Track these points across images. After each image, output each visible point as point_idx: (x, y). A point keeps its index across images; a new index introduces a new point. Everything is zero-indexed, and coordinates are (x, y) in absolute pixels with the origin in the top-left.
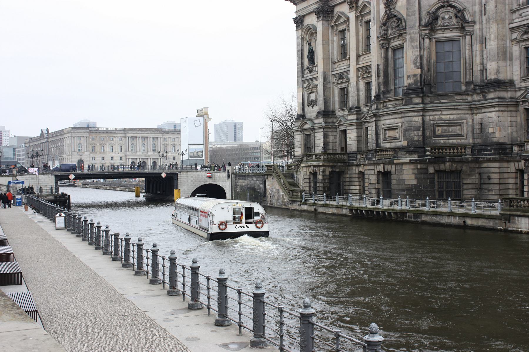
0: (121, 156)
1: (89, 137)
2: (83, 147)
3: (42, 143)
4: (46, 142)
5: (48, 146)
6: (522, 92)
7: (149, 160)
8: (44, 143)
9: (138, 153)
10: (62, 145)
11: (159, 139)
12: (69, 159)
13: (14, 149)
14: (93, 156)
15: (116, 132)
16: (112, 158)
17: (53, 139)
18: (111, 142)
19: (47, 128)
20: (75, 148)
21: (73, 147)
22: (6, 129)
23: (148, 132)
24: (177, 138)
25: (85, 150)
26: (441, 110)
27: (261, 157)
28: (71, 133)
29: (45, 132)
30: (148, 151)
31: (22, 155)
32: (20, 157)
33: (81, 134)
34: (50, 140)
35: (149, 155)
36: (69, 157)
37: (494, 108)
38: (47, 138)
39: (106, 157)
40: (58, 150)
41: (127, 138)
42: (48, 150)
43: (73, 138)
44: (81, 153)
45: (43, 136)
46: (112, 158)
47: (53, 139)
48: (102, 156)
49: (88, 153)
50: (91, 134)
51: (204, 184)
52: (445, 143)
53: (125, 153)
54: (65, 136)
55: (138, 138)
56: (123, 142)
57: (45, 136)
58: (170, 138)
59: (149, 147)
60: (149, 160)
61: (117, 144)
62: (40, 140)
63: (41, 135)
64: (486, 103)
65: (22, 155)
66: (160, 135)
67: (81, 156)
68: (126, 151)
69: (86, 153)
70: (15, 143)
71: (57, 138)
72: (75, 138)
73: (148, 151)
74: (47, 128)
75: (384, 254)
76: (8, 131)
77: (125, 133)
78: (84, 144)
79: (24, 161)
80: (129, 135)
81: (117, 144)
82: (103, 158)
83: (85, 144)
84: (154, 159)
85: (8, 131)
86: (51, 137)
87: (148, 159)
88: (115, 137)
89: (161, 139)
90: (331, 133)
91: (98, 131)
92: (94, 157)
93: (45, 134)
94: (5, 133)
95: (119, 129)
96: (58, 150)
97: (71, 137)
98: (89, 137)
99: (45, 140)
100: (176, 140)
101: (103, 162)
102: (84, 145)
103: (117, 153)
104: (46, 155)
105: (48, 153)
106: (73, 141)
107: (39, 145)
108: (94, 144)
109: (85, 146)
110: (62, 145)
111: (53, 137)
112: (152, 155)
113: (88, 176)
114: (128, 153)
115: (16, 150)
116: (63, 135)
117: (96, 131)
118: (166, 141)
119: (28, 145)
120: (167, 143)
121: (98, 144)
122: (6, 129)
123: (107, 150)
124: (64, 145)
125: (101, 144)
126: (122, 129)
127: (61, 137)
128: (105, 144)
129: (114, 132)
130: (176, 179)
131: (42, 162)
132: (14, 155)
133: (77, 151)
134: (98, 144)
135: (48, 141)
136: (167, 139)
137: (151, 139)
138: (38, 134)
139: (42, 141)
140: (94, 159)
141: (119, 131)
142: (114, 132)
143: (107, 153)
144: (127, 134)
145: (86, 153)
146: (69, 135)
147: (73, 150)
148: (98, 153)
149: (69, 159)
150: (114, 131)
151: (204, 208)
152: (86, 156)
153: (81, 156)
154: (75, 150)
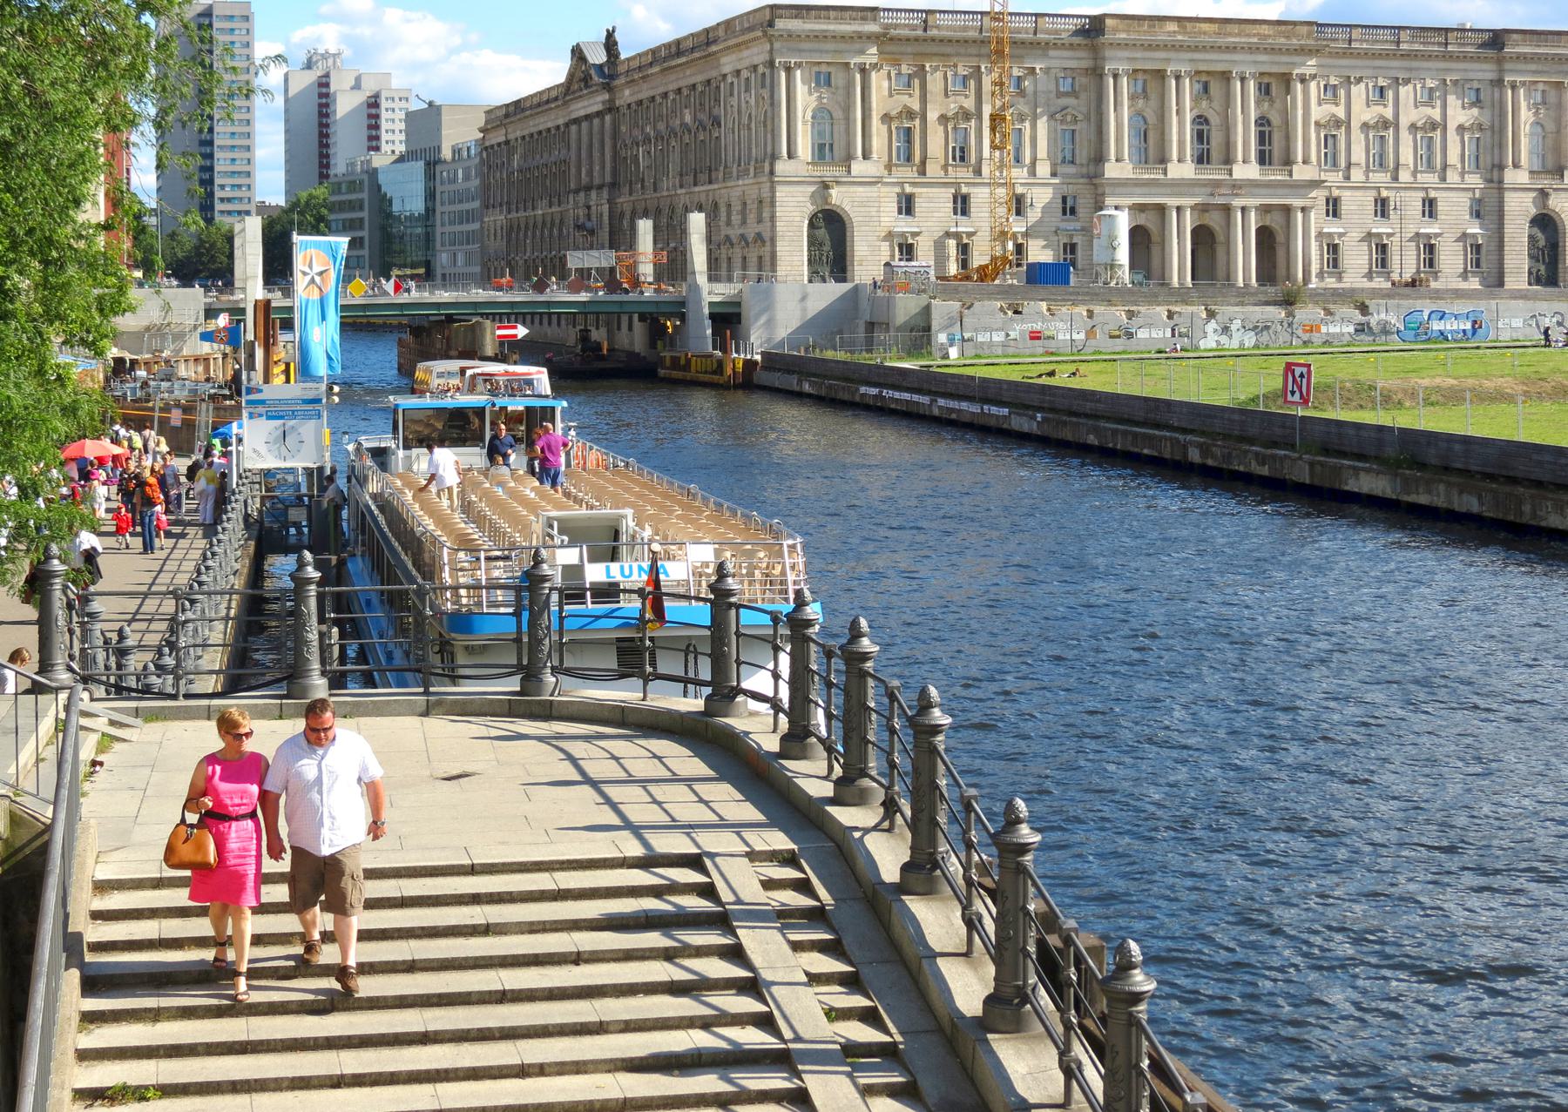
3: (577, 121)
4: (599, 114)
6: (976, 938)
8: (588, 117)
10: (703, 117)
12: (752, 206)
19: (610, 35)
29: (598, 57)
31: (590, 173)
34: (626, 96)
37: (1080, 1065)
38: (608, 87)
39: (980, 196)
40: (675, 158)
63: (571, 76)
64: (579, 140)
65: (590, 173)
74: (610, 35)
79: (476, 226)
96: (675, 158)
104: (600, 187)
112: (1252, 185)
124: (716, 122)
132: (430, 195)
135: (611, 108)
137: (1252, 85)
140: (907, 206)
149: (752, 206)
151: (327, 821)
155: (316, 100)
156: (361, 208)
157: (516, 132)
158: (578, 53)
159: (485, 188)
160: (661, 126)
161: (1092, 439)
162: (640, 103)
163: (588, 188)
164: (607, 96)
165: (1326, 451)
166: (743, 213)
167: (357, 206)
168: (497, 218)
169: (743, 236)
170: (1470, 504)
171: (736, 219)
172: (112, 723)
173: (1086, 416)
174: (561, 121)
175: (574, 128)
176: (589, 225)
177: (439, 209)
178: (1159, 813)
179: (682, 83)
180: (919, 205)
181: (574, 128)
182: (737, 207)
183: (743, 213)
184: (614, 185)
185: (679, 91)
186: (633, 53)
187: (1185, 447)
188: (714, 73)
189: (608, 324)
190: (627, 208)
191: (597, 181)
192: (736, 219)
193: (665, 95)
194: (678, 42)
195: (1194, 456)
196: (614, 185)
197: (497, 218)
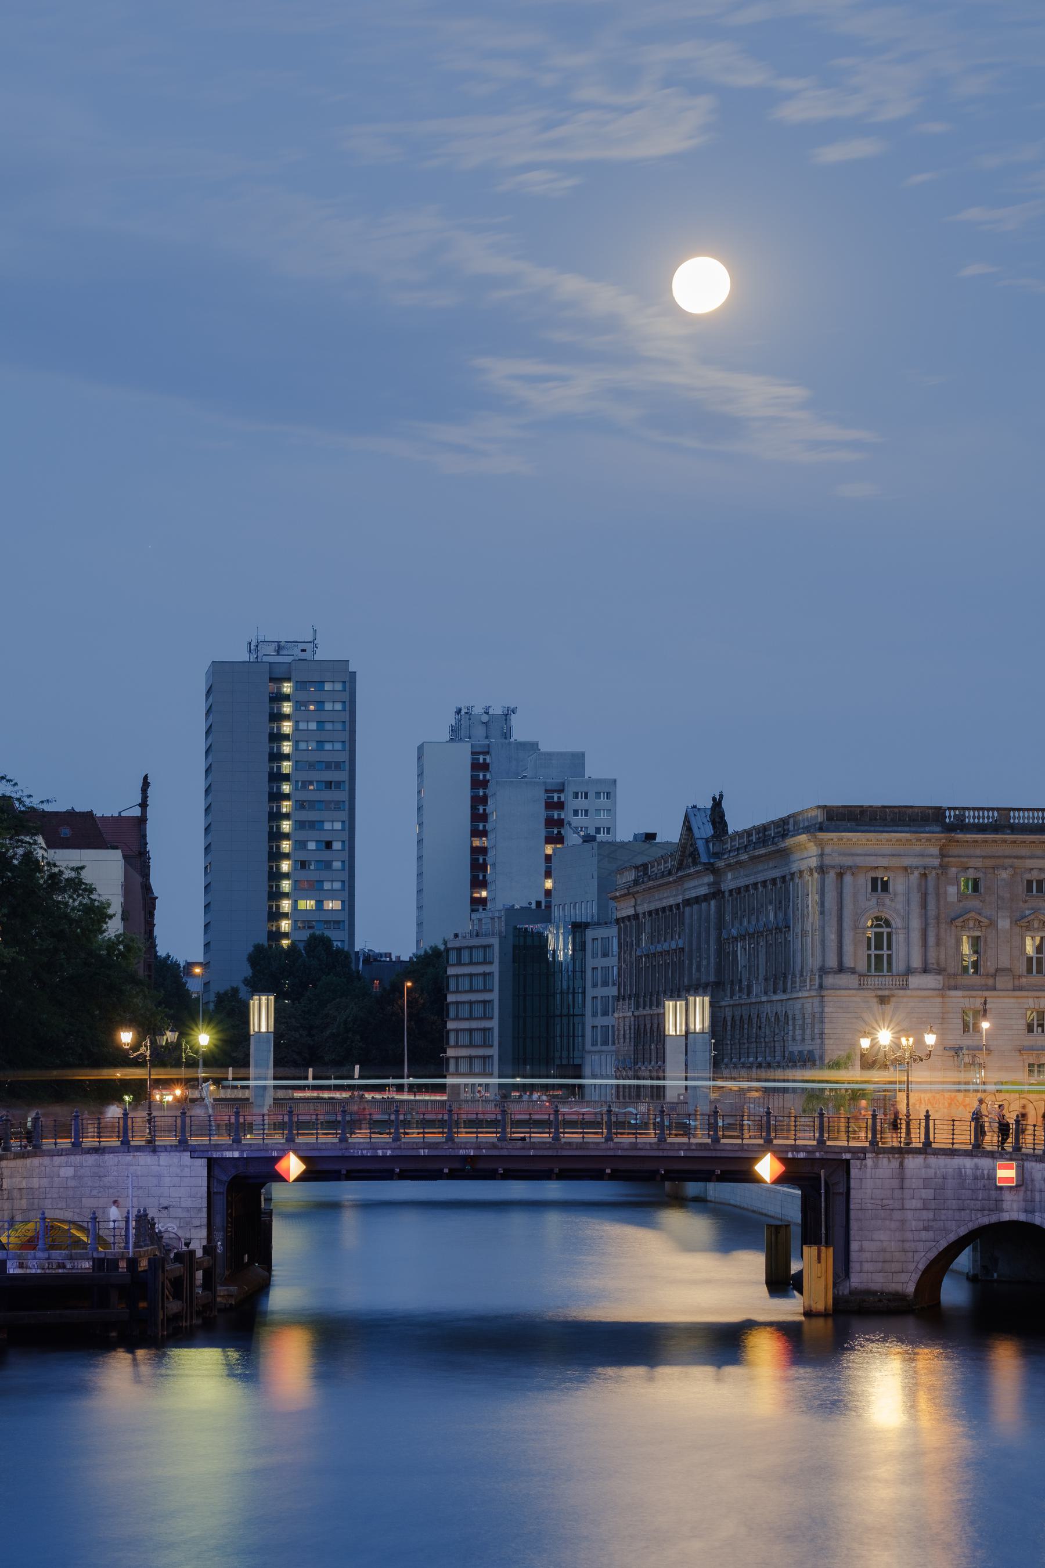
2: (899, 939)
4: (706, 898)
5: (721, 925)
19: (717, 803)
20: (848, 948)
22: (593, 770)
25: (916, 962)
26: (574, 1036)
29: (704, 830)
38: (711, 868)
45: (694, 855)
51: (986, 1221)
52: (634, 1146)
76: (608, 789)
78: (907, 918)
83: (916, 924)
85: (608, 789)
90: (145, 1114)
93: (700, 844)
94: (581, 803)
99: (699, 886)
102: (907, 928)
109: (916, 936)
113: (411, 1166)
121: (1004, 924)
122: (593, 770)
130: (842, 1189)
133: (862, 966)
135: (717, 894)
147: (832, 962)
154: (848, 962)
164: (710, 878)
179: (760, 878)
194: (764, 828)
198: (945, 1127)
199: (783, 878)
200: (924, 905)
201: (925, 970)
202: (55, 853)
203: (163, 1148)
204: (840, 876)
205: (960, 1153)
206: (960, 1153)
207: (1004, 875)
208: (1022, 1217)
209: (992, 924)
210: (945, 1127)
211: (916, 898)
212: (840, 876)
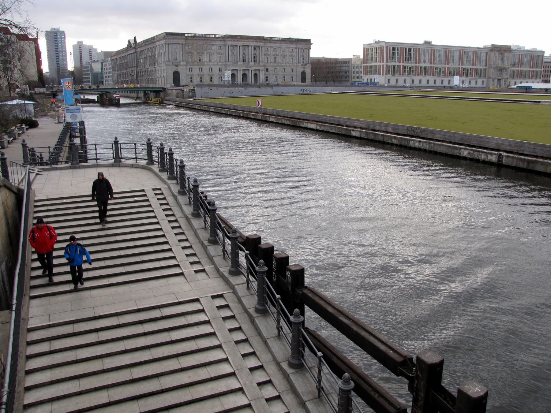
0: (220, 67)
1: (185, 44)
3: (129, 54)
4: (133, 53)
7: (250, 71)
8: (131, 54)
9: (239, 63)
10: (153, 54)
11: (261, 48)
12: (162, 70)
13: (102, 63)
14: (190, 67)
15: (215, 39)
16: (211, 69)
17: (142, 49)
18: (209, 50)
19: (135, 38)
21: (167, 56)
23: (249, 40)
24: (279, 47)
25: (182, 60)
27: (350, 72)
28: (165, 39)
30: (249, 62)
31: (132, 64)
32: (108, 75)
33: (176, 40)
34: (139, 50)
35: (250, 67)
36: (162, 68)
40: (148, 61)
41: (227, 47)
42: (137, 61)
43: (167, 45)
44: (177, 64)
46: (211, 69)
47: (142, 49)
48: (200, 67)
49: (184, 63)
50: (187, 41)
53: (224, 63)
54: (157, 44)
55: (238, 47)
56: (223, 51)
57: (133, 46)
58: (272, 47)
59: (250, 57)
60: (250, 71)
61: (215, 54)
62: (127, 51)
63: (128, 46)
65: (132, 64)
66: (262, 44)
67: (177, 66)
68: (226, 61)
69: (182, 63)
70: (102, 58)
71: (147, 47)
72: (170, 45)
73: (249, 62)
74: (135, 38)
75: (393, 155)
77: (224, 41)
78: (180, 52)
79: (111, 74)
80: (229, 43)
81: (215, 54)
82: (201, 69)
83: (181, 53)
84: (255, 70)
86: (139, 47)
87: (248, 70)
88: (213, 45)
89: (263, 48)
91: (195, 38)
92: (191, 68)
95: (218, 36)
96: (148, 61)
97: (165, 44)
98: (185, 44)
99: (133, 51)
100: (278, 49)
101: (201, 73)
102: (180, 54)
103: (216, 63)
104: (134, 67)
105: (137, 64)
106: (167, 49)
107: (126, 56)
108: (191, 53)
110: (153, 54)
111: (142, 46)
112: (253, 66)
114: (228, 63)
115: (103, 64)
116: (154, 42)
117: (193, 38)
118: (268, 51)
119: (114, 58)
120: (269, 53)
121: (195, 53)
123: (205, 60)
124: (155, 55)
125: (198, 53)
126: (220, 36)
127: (151, 46)
128: (204, 53)
129: (213, 39)
131: (130, 75)
132: (102, 68)
134: (195, 53)
135: (136, 52)
136: (269, 49)
137: (252, 48)
138: (125, 45)
139: (130, 52)
141: (218, 38)
142: (213, 39)
143: (206, 63)
144: (227, 42)
145: (182, 63)
146: (163, 42)
148: (196, 63)
149: (162, 70)
150: (212, 38)
152: (182, 67)
153: (177, 66)
154: (170, 60)
155: (79, 50)
156: (89, 68)
157: (118, 57)
158: (129, 41)
159: (113, 67)
160: (145, 56)
161: (224, 112)
162: (141, 51)
163: (132, 67)
165: (264, 114)
166: (161, 71)
167: (88, 74)
168: (115, 73)
169: (161, 76)
170: (288, 122)
171: (160, 73)
172: (38, 171)
173: (223, 108)
174: (126, 55)
175: (129, 56)
176: (132, 74)
177: (104, 71)
178: (476, 234)
179: (149, 47)
180: (193, 70)
181: (129, 56)
182: (160, 70)
183: (161, 71)
184: (137, 67)
185: (148, 49)
186: (141, 41)
187: (240, 113)
188: (155, 46)
189: (137, 93)
190: (139, 71)
191: (134, 66)
192: (160, 73)
193: (146, 50)
195: (242, 115)
196: (137, 67)
197: (115, 73)
198: (15, 170)
199: (154, 47)
200: (182, 50)
201: (183, 61)
202: (164, 354)
203: (134, 166)
204: (168, 45)
205: (36, 45)
206: (36, 45)
207: (195, 45)
208: (16, 392)
209: (193, 53)
210: (15, 170)
211: (181, 49)
212: (168, 45)
